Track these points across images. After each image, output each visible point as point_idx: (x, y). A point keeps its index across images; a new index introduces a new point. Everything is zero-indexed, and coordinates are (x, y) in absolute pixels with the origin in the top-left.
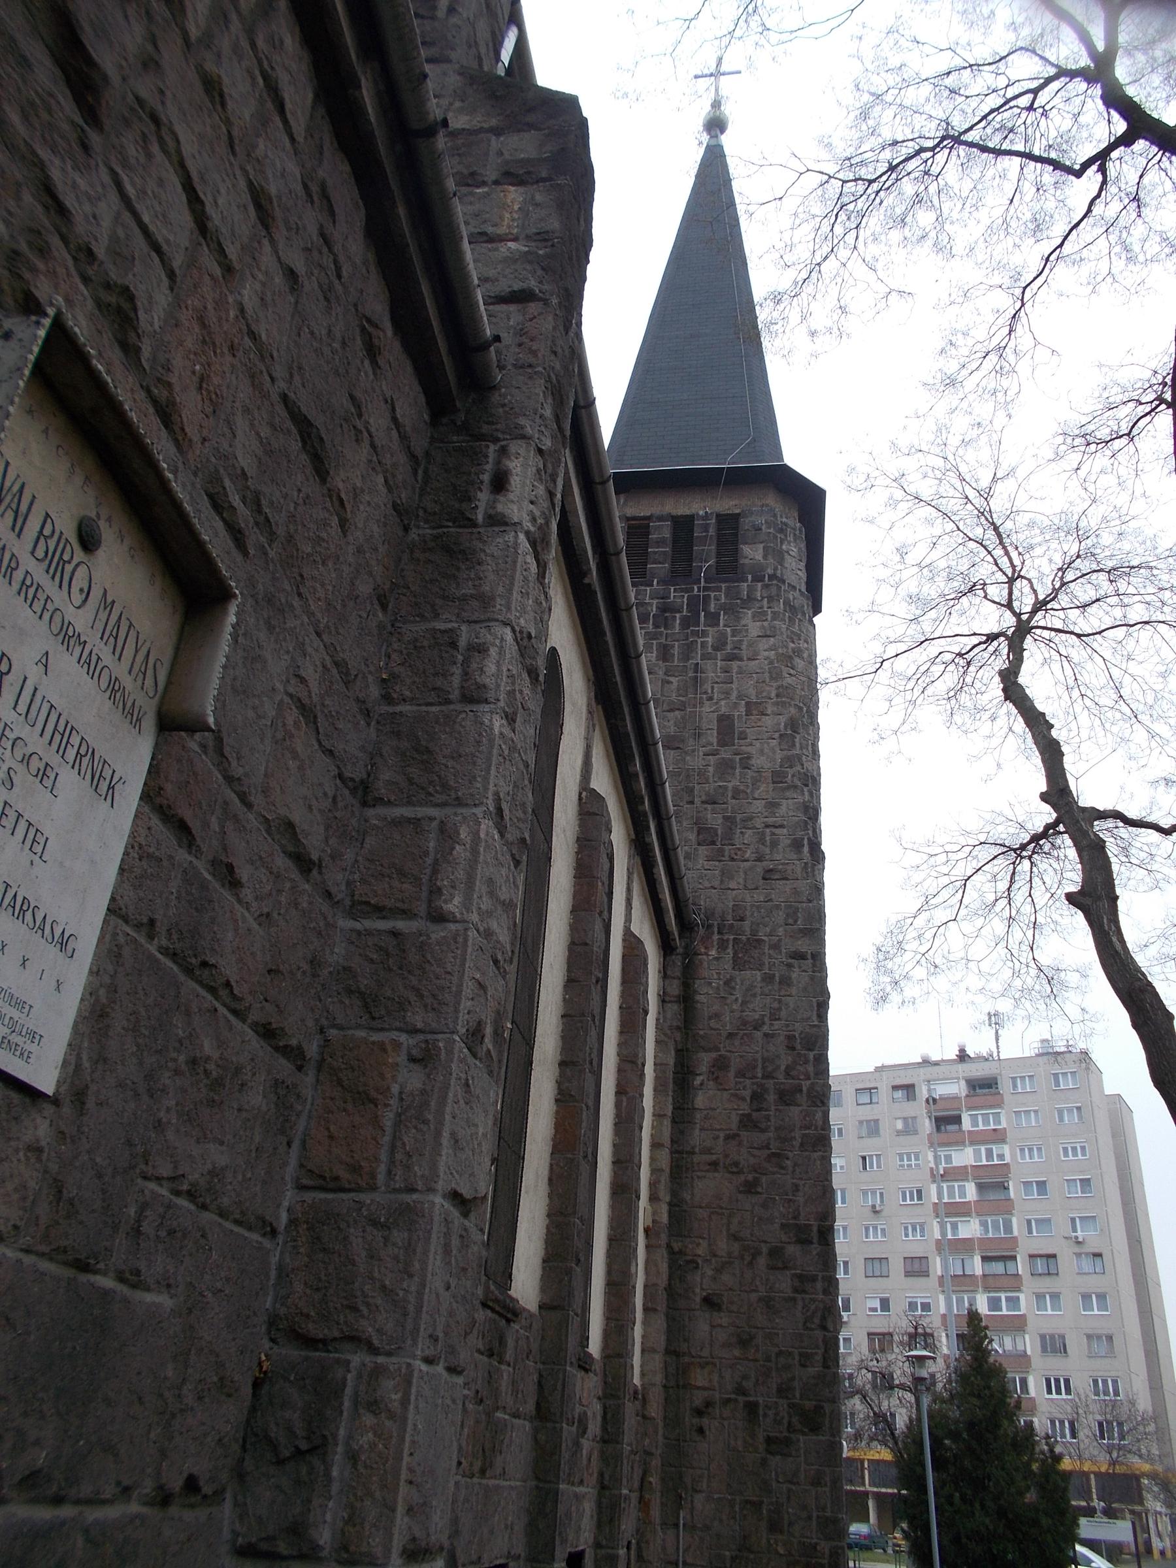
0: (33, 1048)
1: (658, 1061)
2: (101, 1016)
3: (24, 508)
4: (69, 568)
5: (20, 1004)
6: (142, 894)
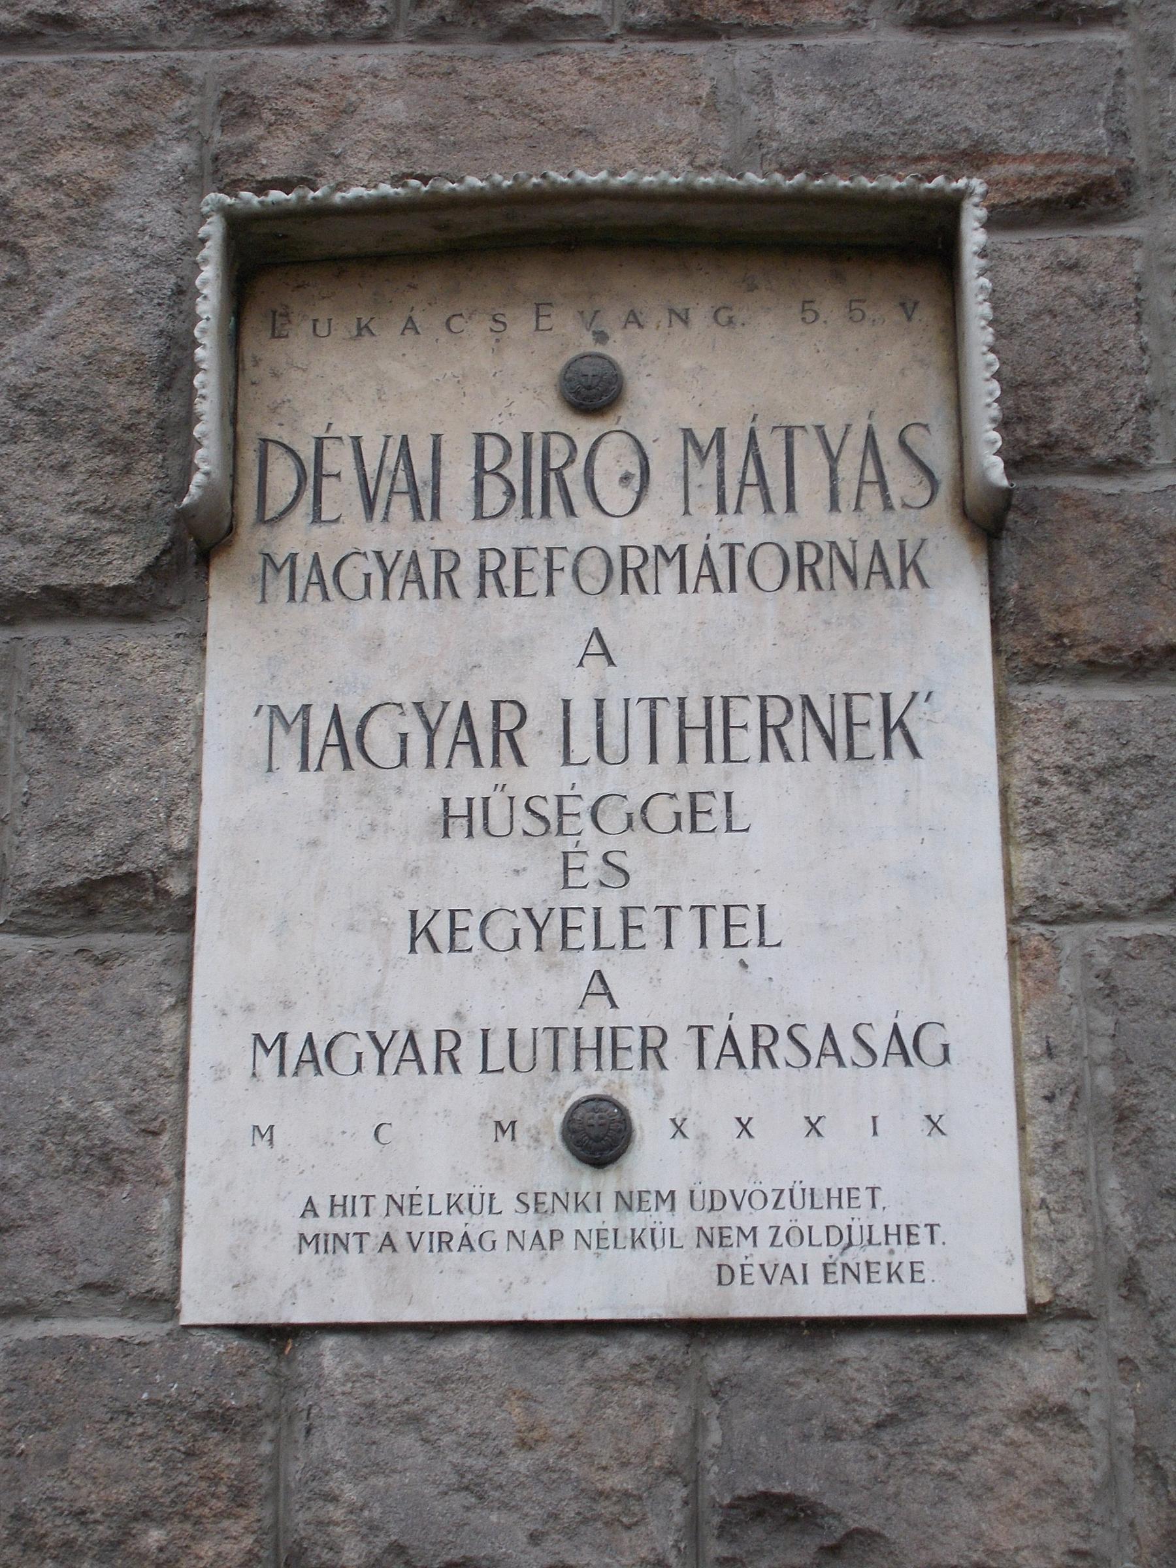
0: (922, 1251)
1: (146, 952)
2: (1121, 1119)
3: (422, 469)
4: (575, 474)
5: (847, 1196)
6: (1133, 847)
